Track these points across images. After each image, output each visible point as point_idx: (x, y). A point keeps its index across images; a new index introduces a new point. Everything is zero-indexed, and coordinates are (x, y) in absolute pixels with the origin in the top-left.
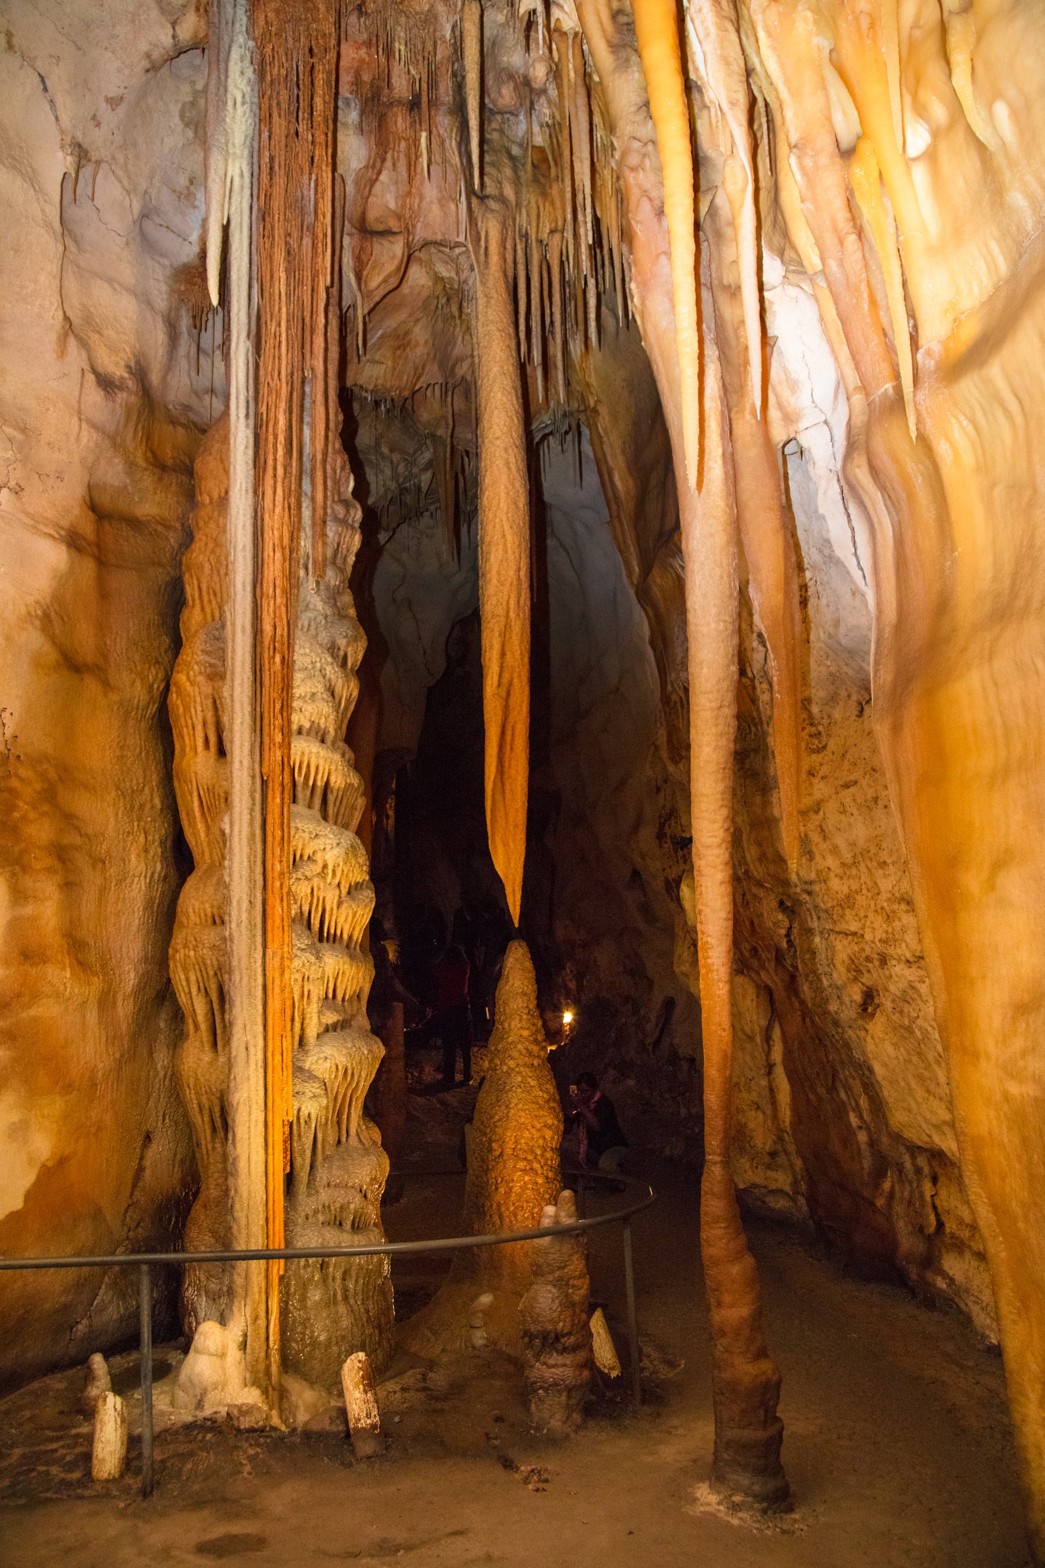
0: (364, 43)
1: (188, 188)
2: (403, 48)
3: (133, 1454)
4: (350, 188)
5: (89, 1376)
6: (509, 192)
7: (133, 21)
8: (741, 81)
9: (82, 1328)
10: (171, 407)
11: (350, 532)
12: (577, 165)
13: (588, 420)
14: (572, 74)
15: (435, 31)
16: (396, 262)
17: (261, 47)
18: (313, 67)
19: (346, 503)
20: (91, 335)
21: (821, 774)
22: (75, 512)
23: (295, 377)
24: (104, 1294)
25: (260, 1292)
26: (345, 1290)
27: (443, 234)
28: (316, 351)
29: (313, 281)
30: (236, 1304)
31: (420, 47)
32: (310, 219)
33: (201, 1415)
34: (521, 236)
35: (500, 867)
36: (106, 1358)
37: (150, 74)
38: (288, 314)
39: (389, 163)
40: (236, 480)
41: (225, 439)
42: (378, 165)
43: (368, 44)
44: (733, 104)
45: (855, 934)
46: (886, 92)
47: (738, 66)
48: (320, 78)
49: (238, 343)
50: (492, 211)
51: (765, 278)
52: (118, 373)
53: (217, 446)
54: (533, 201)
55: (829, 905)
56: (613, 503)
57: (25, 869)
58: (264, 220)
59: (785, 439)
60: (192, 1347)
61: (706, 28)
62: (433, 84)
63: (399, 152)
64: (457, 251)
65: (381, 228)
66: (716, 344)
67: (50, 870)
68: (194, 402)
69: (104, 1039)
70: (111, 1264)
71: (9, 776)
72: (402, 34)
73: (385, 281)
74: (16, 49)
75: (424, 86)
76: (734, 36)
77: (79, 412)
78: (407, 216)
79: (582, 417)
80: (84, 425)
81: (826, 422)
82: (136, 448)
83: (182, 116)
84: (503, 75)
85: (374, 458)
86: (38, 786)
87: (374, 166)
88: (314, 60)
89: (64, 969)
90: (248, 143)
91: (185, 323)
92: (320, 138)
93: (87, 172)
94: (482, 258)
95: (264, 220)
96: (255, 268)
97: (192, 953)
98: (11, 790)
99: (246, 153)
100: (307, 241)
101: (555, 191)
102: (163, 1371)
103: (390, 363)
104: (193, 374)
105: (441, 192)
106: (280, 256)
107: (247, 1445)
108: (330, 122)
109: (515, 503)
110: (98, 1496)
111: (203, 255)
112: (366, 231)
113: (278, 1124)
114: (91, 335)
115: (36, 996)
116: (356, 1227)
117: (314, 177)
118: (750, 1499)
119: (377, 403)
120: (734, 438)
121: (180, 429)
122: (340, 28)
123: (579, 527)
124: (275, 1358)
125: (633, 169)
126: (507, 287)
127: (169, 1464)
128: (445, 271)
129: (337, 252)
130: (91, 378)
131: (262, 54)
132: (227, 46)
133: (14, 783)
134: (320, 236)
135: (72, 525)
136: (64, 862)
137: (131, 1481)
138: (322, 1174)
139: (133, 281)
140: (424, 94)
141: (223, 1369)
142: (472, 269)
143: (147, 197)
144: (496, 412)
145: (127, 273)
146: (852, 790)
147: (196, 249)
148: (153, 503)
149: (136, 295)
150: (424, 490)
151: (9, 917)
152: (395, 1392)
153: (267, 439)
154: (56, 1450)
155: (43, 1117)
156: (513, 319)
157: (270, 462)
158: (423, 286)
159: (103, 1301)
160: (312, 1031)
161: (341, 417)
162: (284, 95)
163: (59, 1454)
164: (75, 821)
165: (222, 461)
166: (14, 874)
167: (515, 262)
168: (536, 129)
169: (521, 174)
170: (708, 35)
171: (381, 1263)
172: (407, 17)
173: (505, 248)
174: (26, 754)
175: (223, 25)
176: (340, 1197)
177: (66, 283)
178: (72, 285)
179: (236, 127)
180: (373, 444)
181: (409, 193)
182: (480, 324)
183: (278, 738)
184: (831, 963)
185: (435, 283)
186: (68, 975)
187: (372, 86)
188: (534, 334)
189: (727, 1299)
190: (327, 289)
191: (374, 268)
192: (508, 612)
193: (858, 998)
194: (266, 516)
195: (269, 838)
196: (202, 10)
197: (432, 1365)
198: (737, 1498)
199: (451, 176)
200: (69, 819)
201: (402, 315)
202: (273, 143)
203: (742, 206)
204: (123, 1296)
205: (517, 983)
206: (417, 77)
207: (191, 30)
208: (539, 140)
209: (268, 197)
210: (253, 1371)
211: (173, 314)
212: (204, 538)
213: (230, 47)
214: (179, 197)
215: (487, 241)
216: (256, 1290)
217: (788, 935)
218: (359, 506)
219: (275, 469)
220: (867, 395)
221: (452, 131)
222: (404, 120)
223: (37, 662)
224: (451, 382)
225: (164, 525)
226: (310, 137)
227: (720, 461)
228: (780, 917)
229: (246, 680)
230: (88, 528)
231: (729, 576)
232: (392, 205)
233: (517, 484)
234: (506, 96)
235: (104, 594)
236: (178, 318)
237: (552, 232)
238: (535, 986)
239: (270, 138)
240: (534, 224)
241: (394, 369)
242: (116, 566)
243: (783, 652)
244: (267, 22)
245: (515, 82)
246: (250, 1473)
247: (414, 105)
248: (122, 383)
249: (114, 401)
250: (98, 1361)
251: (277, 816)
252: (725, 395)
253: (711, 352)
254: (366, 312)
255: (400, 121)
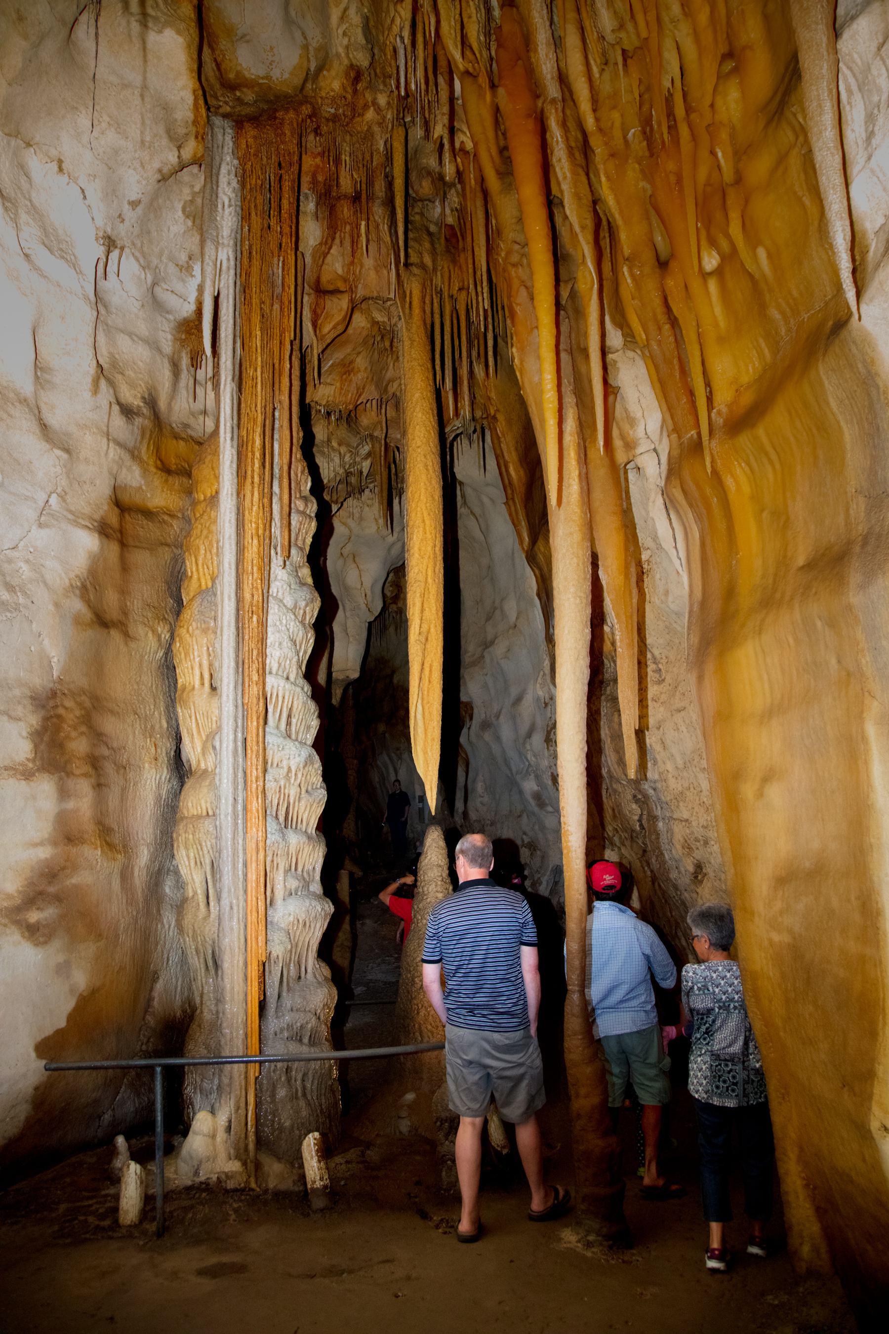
0: (319, 154)
1: (188, 263)
2: (348, 158)
3: (148, 1208)
4: (308, 259)
5: (113, 1152)
6: (428, 260)
7: (149, 148)
8: (589, 211)
9: (107, 1117)
10: (174, 425)
11: (308, 520)
12: (476, 249)
13: (489, 425)
14: (473, 182)
15: (372, 145)
16: (343, 313)
17: (243, 164)
18: (281, 177)
19: (305, 499)
20: (116, 375)
21: (661, 700)
22: (105, 508)
23: (267, 409)
24: (124, 1093)
25: (241, 1089)
26: (304, 1088)
27: (378, 293)
28: (283, 389)
29: (281, 336)
30: (223, 1097)
31: (360, 158)
32: (278, 290)
33: (197, 1180)
34: (437, 293)
35: (420, 770)
36: (127, 1139)
37: (161, 184)
38: (262, 362)
39: (337, 241)
40: (224, 487)
41: (216, 453)
42: (329, 242)
43: (322, 154)
44: (583, 228)
45: (687, 820)
46: (689, 225)
47: (587, 199)
48: (286, 185)
49: (225, 384)
50: (415, 275)
51: (609, 343)
52: (136, 403)
53: (209, 457)
54: (446, 266)
55: (668, 799)
56: (508, 488)
57: (69, 774)
58: (245, 292)
59: (626, 461)
60: (191, 1129)
61: (564, 173)
62: (370, 183)
63: (344, 233)
64: (389, 303)
65: (331, 288)
66: (575, 393)
67: (86, 775)
68: (191, 421)
69: (124, 901)
70: (129, 1067)
71: (57, 706)
72: (347, 149)
73: (334, 327)
74: (65, 171)
75: (364, 186)
76: (584, 178)
77: (108, 435)
78: (351, 279)
79: (485, 423)
80: (111, 444)
81: (655, 450)
82: (148, 458)
83: (184, 210)
84: (423, 172)
85: (326, 450)
86: (78, 713)
87: (326, 243)
88: (283, 172)
89: (96, 848)
90: (233, 235)
91: (185, 361)
92: (287, 230)
93: (114, 255)
94: (407, 311)
95: (245, 292)
96: (238, 328)
97: (191, 836)
98: (59, 717)
99: (232, 242)
100: (276, 306)
101: (462, 259)
102: (171, 1150)
103: (338, 385)
104: (191, 400)
105: (376, 261)
106: (256, 319)
107: (231, 1201)
108: (294, 217)
109: (432, 496)
110: (124, 1237)
111: (199, 312)
112: (320, 291)
113: (255, 964)
114: (116, 375)
115: (75, 868)
116: (313, 1042)
117: (281, 259)
118: (600, 1238)
119: (329, 414)
120: (588, 461)
121: (182, 443)
122: (301, 147)
123: (486, 500)
124: (252, 1137)
125: (514, 265)
126: (426, 333)
127: (175, 1214)
128: (379, 317)
129: (299, 311)
130: (116, 408)
131: (243, 170)
132: (218, 164)
133: (61, 711)
134: (287, 303)
135: (102, 518)
136: (96, 769)
137: (148, 1226)
138: (287, 1002)
139: (147, 334)
140: (364, 192)
141: (214, 1145)
142: (400, 319)
143: (157, 271)
144: (418, 427)
145: (142, 328)
146: (683, 713)
147: (193, 307)
148: (159, 496)
149: (149, 344)
150: (365, 474)
151: (56, 811)
152: (341, 1164)
153: (247, 455)
154: (91, 1206)
155: (81, 958)
156: (430, 356)
157: (249, 473)
158: (363, 328)
159: (123, 1097)
160: (279, 893)
161: (301, 434)
162: (260, 199)
163: (94, 1208)
164: (104, 738)
165: (213, 468)
166: (61, 779)
167: (432, 313)
168: (448, 211)
169: (437, 246)
170: (565, 178)
171: (331, 1067)
172: (351, 135)
173: (424, 302)
174: (69, 690)
175: (215, 149)
176: (299, 1019)
177: (98, 338)
178: (101, 339)
179: (224, 223)
180: (326, 439)
181: (352, 263)
182: (406, 360)
183: (255, 677)
184: (671, 842)
185: (372, 326)
186: (99, 853)
187: (325, 185)
188: (446, 366)
189: (583, 1091)
190: (292, 342)
191: (326, 318)
192: (426, 579)
193: (691, 869)
194: (247, 513)
195: (249, 751)
196: (200, 138)
197: (369, 1145)
198: (591, 1238)
199: (384, 250)
200: (98, 736)
201: (348, 349)
202: (251, 234)
203: (590, 300)
204: (138, 1094)
205: (434, 858)
206: (359, 180)
207: (192, 152)
208: (450, 220)
209: (248, 274)
210: (237, 1149)
211: (176, 356)
212: (200, 526)
213: (220, 164)
214: (181, 270)
215: (411, 297)
216: (238, 1087)
217: (640, 821)
218: (315, 501)
219: (253, 477)
220: (679, 437)
221: (384, 217)
222: (349, 210)
223: (77, 621)
224: (385, 397)
225: (170, 515)
226: (279, 228)
227: (577, 480)
228: (634, 806)
229: (231, 635)
230: (114, 520)
231: (583, 564)
232: (340, 272)
233: (434, 482)
234: (425, 187)
235: (125, 567)
236: (180, 358)
237: (460, 289)
238: (447, 860)
239: (249, 230)
240: (447, 284)
241: (342, 389)
242: (136, 547)
243: (623, 618)
244: (247, 146)
245: (432, 177)
246: (235, 1221)
247: (356, 199)
248: (139, 410)
249: (133, 424)
250: (120, 1140)
251: (254, 736)
252: (581, 430)
253: (570, 400)
254: (320, 351)
255: (345, 211)
